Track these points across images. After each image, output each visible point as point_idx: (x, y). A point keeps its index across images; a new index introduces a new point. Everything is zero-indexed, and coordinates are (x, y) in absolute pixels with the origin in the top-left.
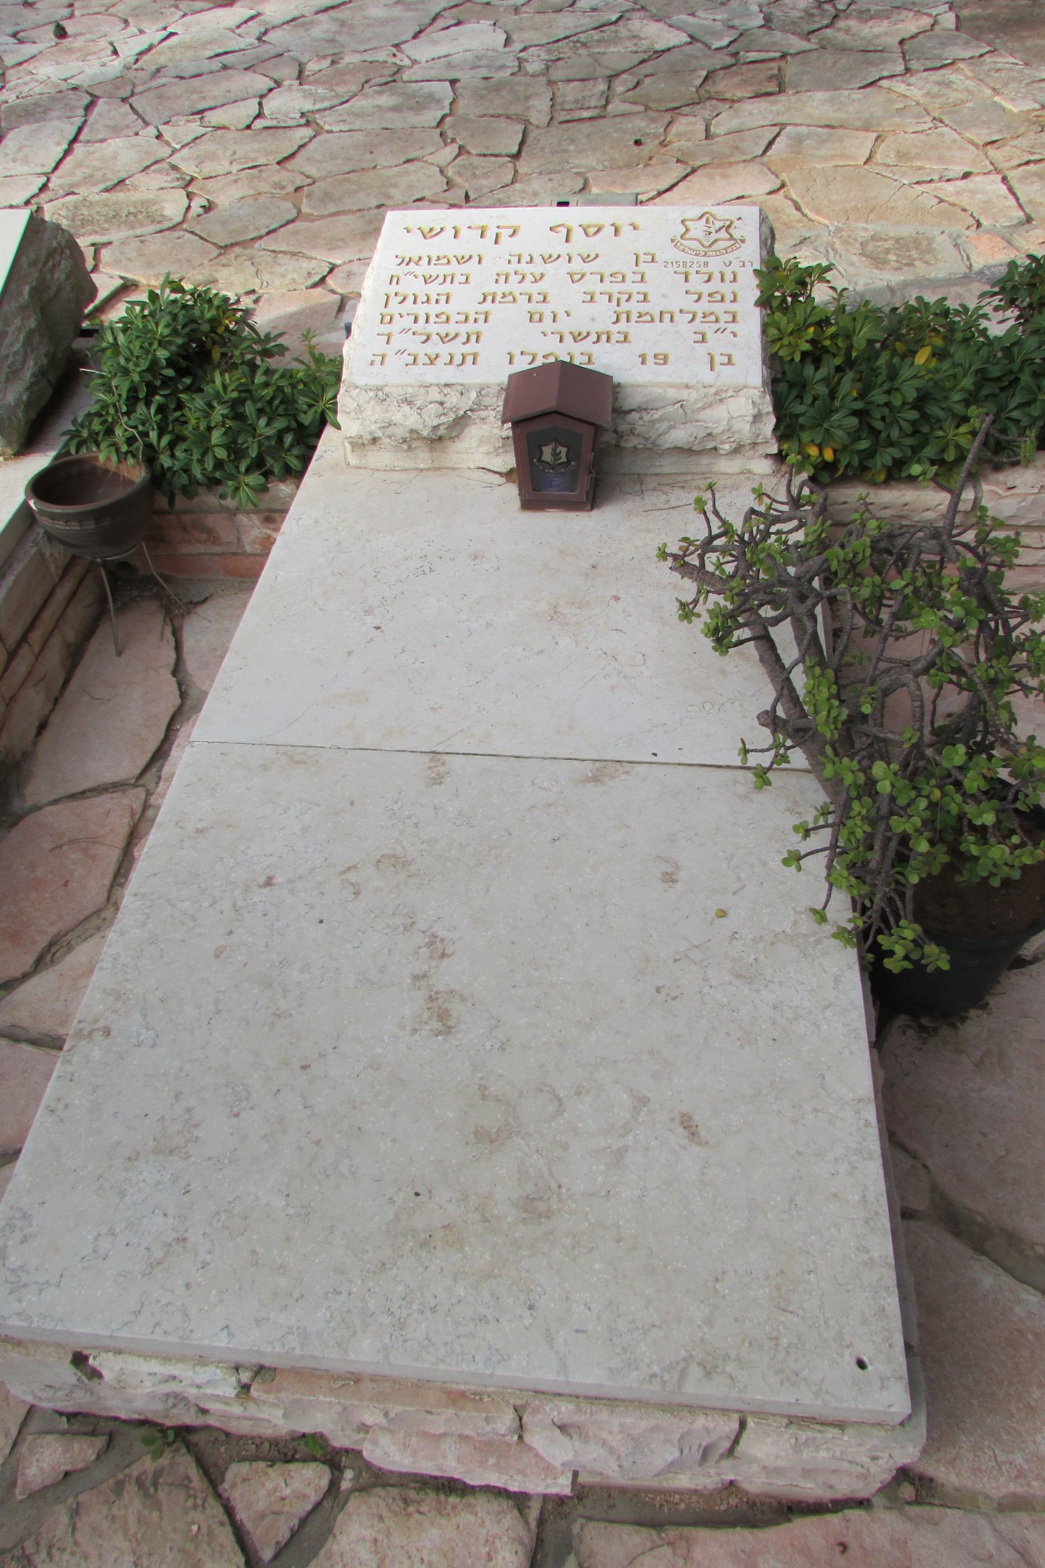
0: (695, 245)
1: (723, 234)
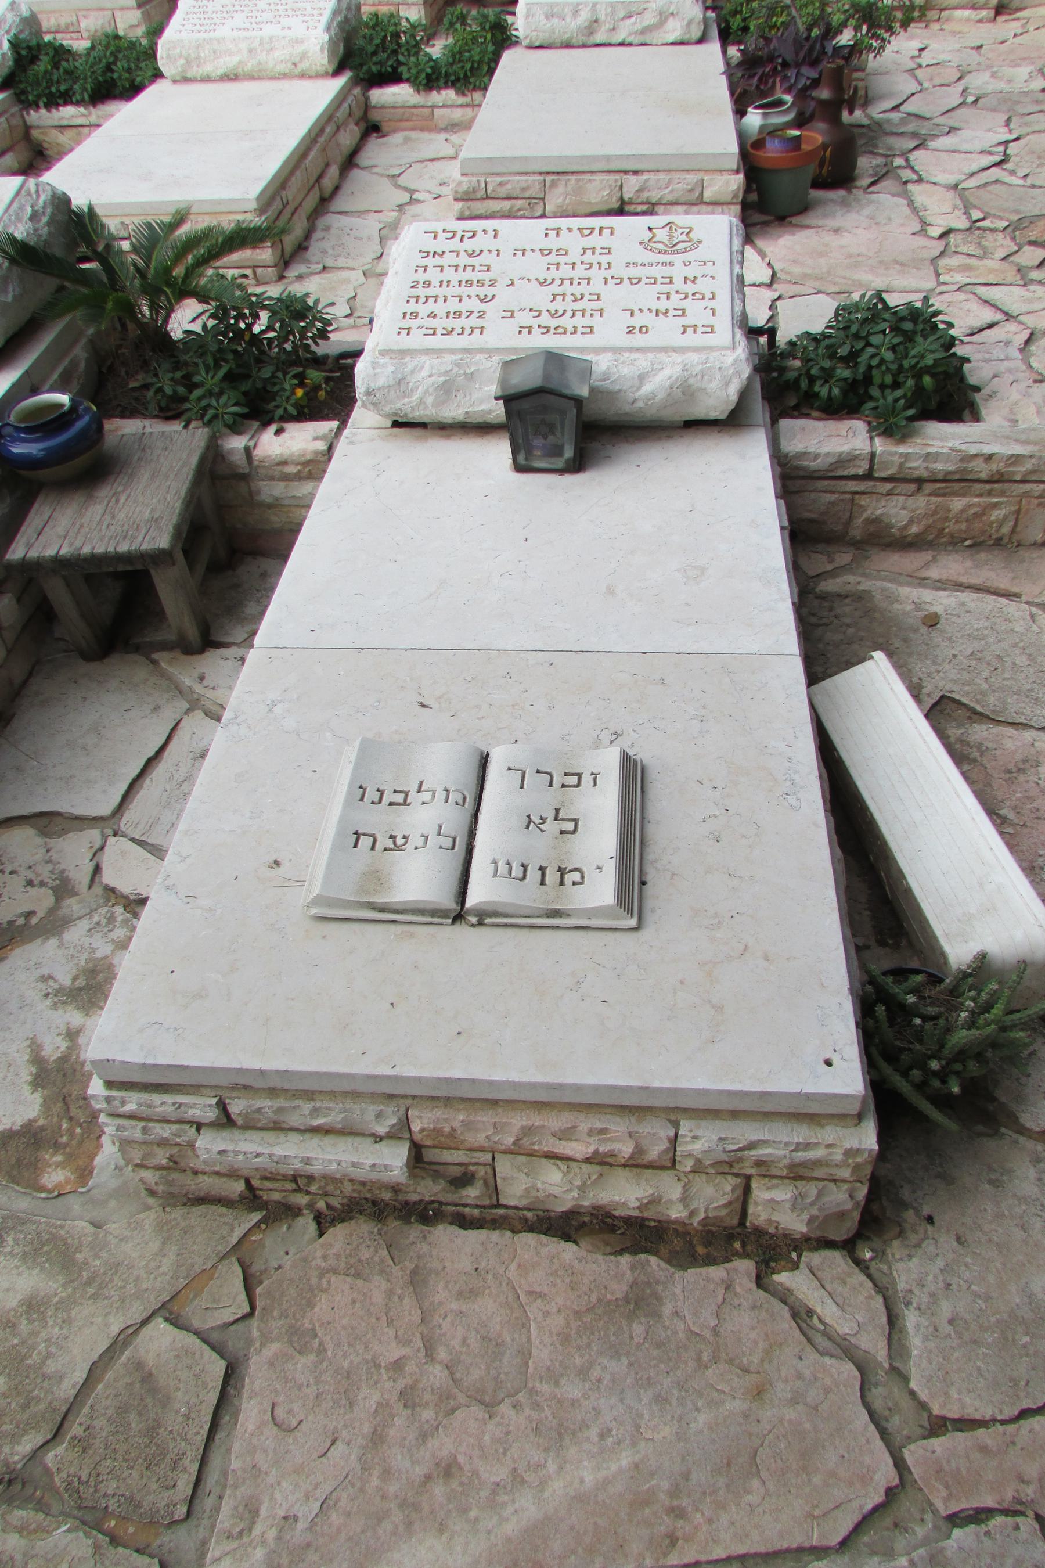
0: (660, 246)
1: (684, 237)
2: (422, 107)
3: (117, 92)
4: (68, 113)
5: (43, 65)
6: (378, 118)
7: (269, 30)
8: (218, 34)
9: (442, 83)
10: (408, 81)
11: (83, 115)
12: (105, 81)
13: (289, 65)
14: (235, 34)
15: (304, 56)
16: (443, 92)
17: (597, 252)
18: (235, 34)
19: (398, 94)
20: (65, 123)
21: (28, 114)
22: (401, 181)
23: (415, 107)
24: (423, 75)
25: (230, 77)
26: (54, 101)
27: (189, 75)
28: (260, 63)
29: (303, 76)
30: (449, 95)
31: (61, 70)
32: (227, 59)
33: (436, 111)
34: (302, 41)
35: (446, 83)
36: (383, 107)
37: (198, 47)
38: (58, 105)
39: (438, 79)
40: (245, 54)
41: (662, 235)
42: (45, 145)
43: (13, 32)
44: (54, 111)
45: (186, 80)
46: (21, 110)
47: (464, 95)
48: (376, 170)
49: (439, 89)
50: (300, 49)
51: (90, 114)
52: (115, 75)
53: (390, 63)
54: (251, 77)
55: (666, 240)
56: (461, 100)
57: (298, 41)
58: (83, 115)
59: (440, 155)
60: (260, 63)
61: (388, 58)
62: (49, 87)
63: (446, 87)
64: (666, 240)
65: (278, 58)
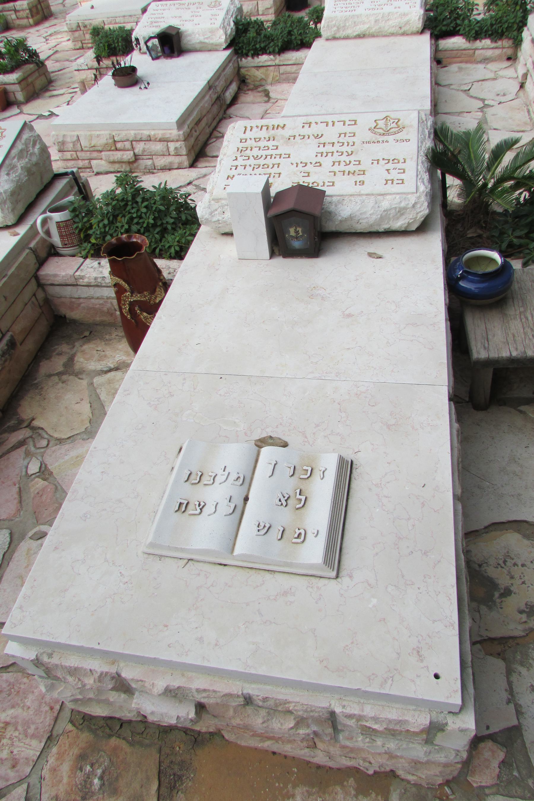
0: (381, 131)
1: (394, 125)
2: (469, 49)
3: (292, 46)
4: (264, 59)
5: (252, 34)
6: (442, 57)
7: (387, 9)
8: (357, 13)
9: (483, 35)
10: (461, 35)
11: (271, 60)
12: (288, 41)
13: (397, 28)
14: (368, 12)
15: (407, 23)
16: (483, 41)
17: (282, 157)
18: (368, 12)
19: (456, 42)
20: (261, 64)
21: (241, 60)
22: (471, 92)
23: (464, 50)
24: (474, 31)
25: (359, 37)
26: (256, 53)
27: (337, 36)
28: (380, 28)
29: (404, 34)
30: (487, 42)
31: (262, 36)
32: (362, 26)
33: (477, 52)
34: (407, 15)
35: (485, 35)
36: (445, 50)
37: (345, 20)
38: (258, 55)
39: (481, 34)
40: (373, 23)
41: (381, 124)
42: (247, 77)
43: (234, 16)
44: (256, 58)
45: (334, 38)
46: (238, 58)
47: (496, 42)
48: (452, 87)
49: (481, 39)
50: (406, 19)
51: (276, 59)
52: (293, 37)
53: (452, 25)
54: (373, 36)
55: (383, 126)
56: (494, 45)
57: (405, 15)
58: (271, 60)
59: (487, 78)
60: (380, 28)
61: (451, 22)
62: (255, 45)
63: (485, 38)
64: (383, 126)
65: (391, 25)
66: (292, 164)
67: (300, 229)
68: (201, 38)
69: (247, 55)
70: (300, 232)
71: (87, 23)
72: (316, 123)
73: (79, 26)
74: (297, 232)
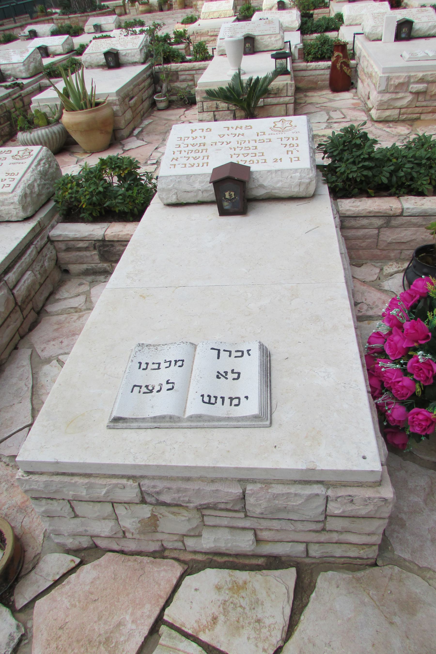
1: (288, 125)
66: (231, 149)
67: (233, 193)
68: (287, 25)
69: (307, 34)
70: (233, 195)
71: (198, 31)
72: (228, 135)
73: (194, 33)
74: (230, 195)
